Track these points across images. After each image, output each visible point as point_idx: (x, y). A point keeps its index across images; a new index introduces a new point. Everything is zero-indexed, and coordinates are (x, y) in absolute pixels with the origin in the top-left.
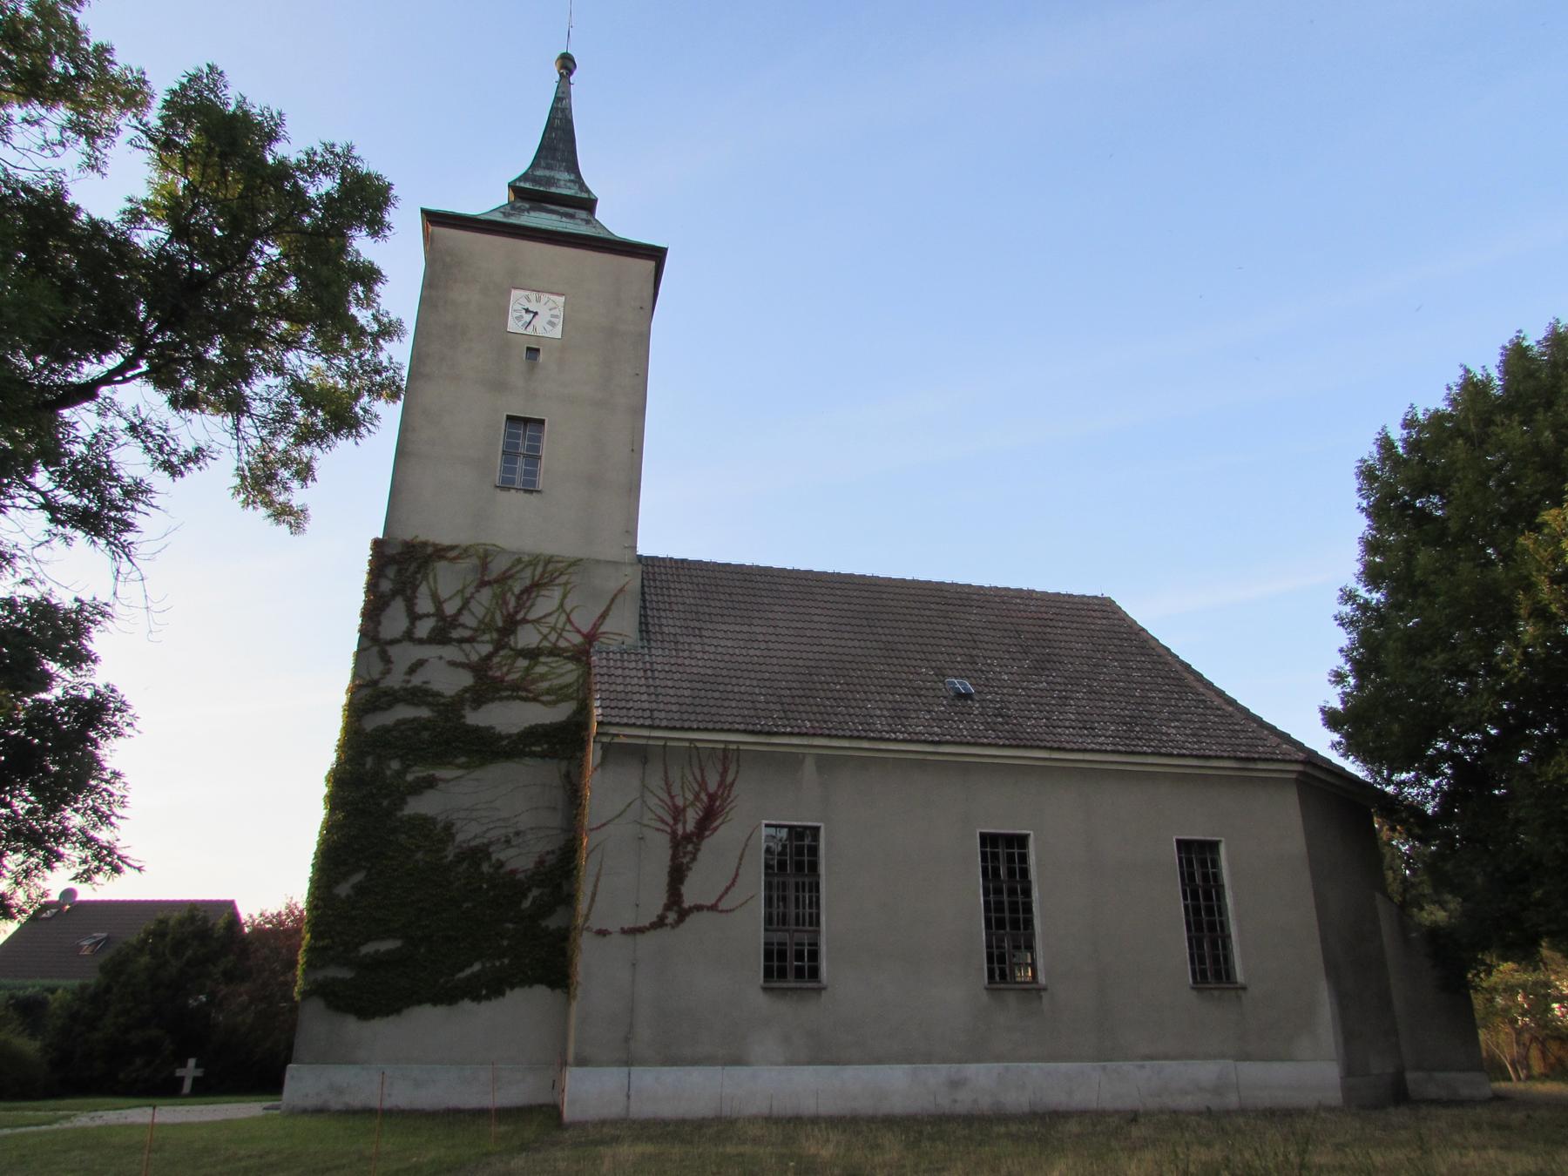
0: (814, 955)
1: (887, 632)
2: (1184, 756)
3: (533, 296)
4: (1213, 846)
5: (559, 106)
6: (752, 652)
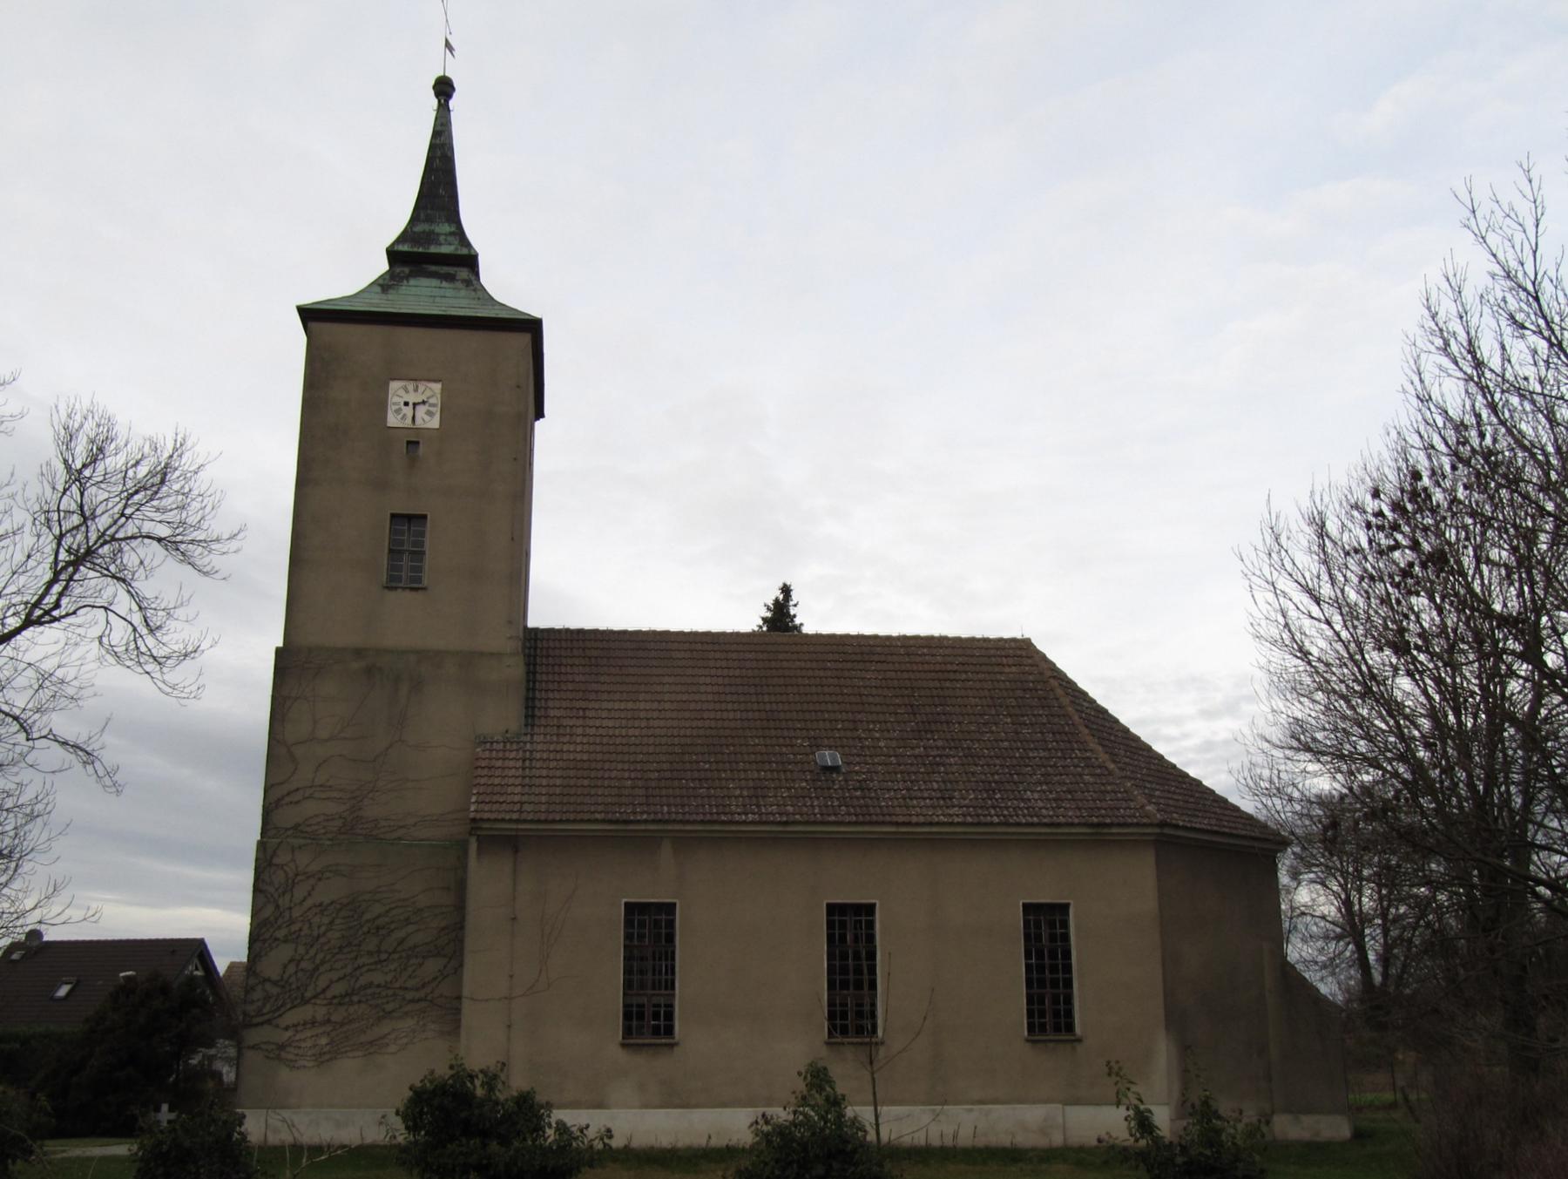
0: (669, 1016)
1: (773, 698)
3: (411, 386)
4: (1064, 908)
6: (631, 732)
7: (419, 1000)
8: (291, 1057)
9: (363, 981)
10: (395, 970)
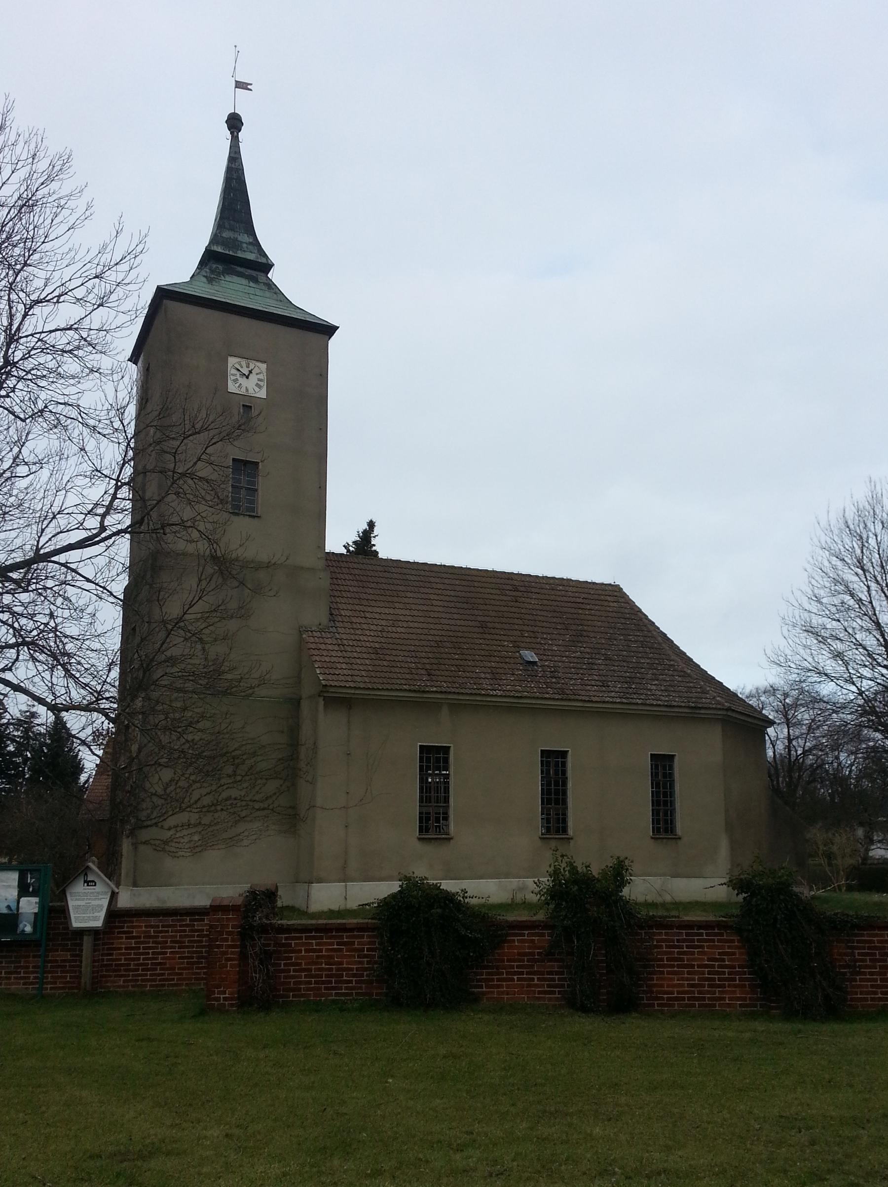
2: (659, 705)
5: (233, 166)
7: (264, 809)
8: (173, 849)
9: (224, 795)
10: (247, 788)
